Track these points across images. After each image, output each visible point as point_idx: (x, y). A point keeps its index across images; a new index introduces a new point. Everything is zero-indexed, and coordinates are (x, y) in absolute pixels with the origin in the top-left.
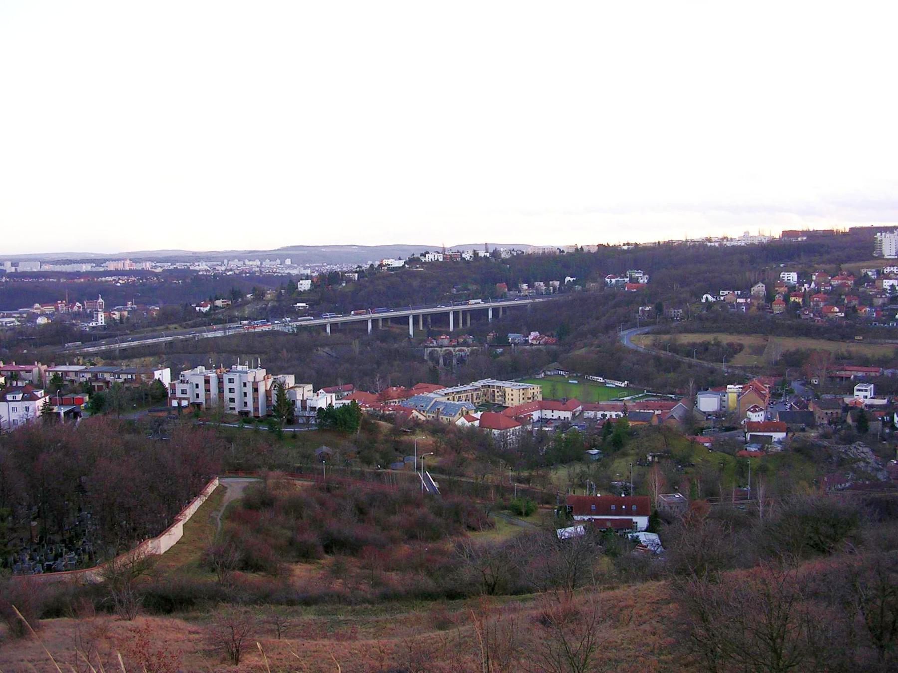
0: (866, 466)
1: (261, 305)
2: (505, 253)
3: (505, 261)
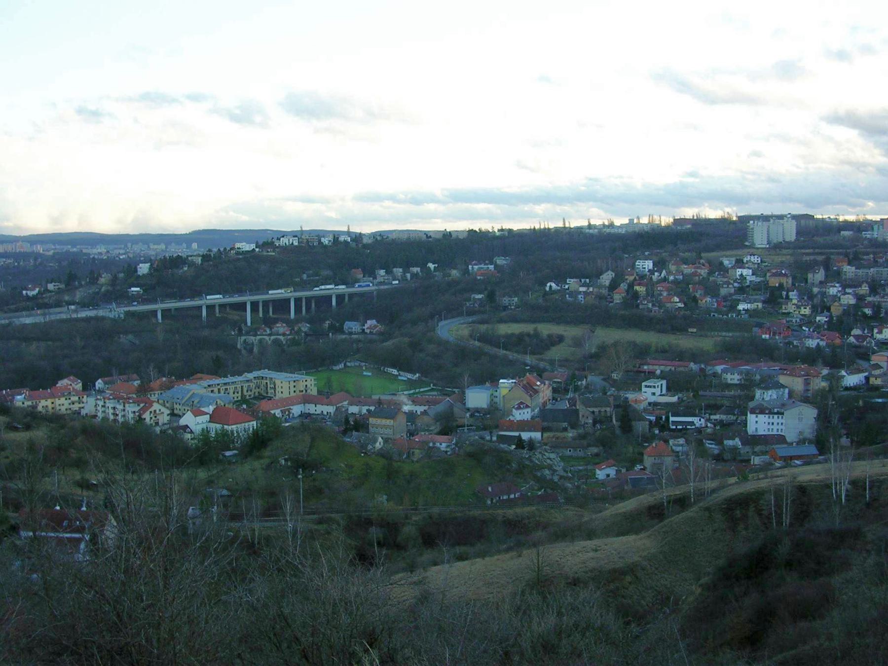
0: (552, 475)
1: (93, 289)
2: (368, 238)
3: (366, 246)
